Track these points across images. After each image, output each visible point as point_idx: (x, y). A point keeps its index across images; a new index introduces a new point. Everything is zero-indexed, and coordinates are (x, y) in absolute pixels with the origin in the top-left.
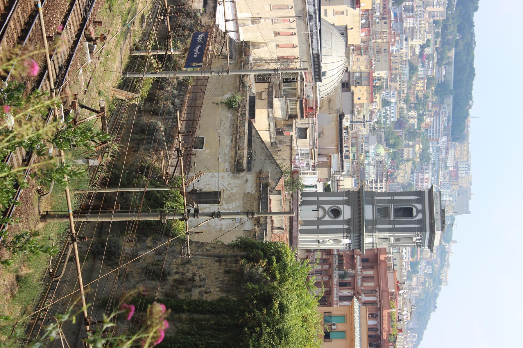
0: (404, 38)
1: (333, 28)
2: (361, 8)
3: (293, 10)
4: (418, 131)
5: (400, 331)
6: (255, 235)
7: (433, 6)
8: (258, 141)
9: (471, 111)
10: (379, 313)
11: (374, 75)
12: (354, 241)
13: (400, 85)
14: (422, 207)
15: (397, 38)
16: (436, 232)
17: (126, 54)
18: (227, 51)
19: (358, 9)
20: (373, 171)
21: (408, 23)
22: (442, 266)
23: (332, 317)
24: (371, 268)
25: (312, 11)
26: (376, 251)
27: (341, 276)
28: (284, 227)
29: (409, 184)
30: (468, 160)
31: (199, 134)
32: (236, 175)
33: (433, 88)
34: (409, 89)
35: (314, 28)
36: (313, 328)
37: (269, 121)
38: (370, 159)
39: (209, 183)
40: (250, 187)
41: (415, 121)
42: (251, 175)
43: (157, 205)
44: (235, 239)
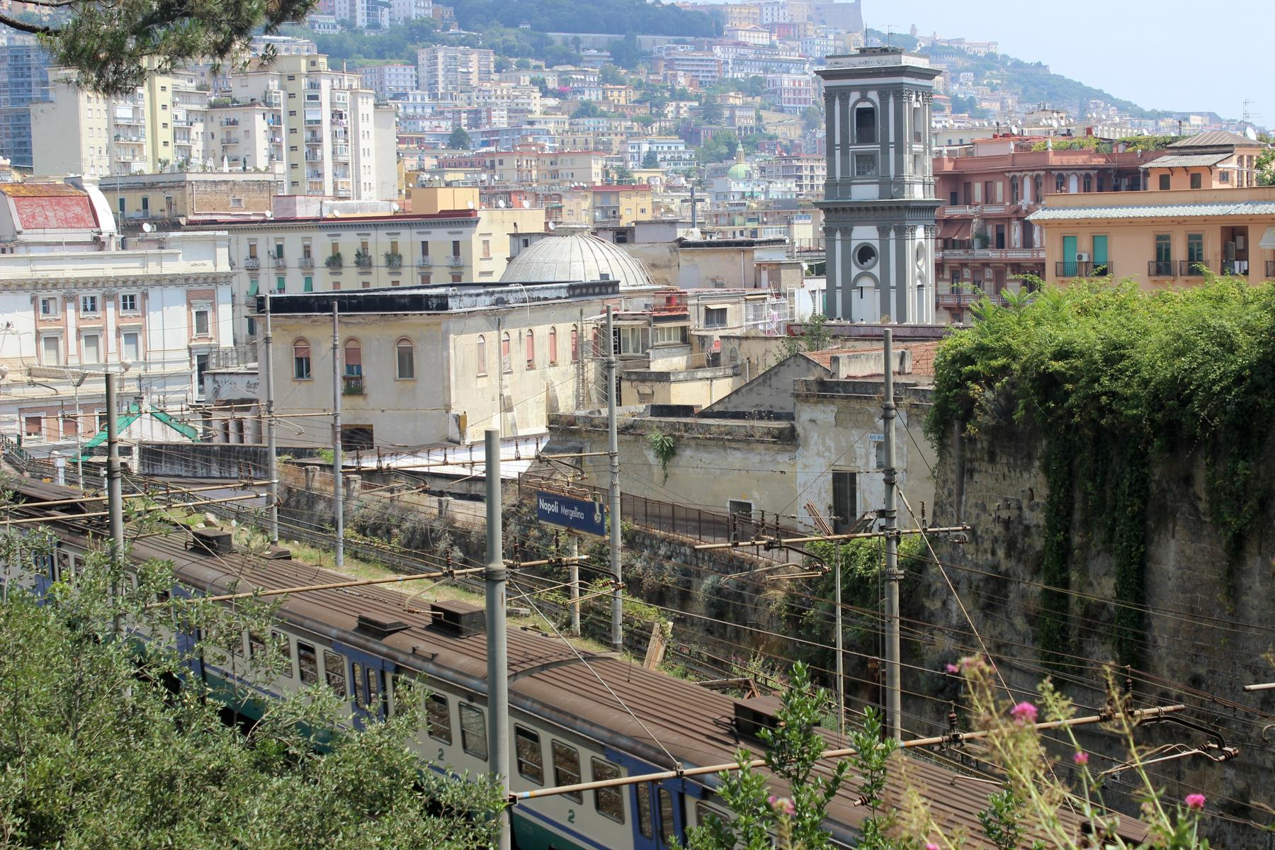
0: (529, 127)
1: (518, 260)
2: (477, 208)
3: (486, 334)
4: (703, 100)
5: (1089, 131)
6: (917, 406)
7: (469, 73)
8: (734, 398)
10: (1056, 173)
11: (599, 184)
13: (616, 135)
14: (855, 90)
15: (530, 140)
16: (903, 64)
18: (567, 457)
19: (479, 214)
20: (779, 185)
21: (500, 120)
22: (960, 53)
23: (1067, 260)
24: (968, 186)
26: (938, 178)
27: (985, 244)
28: (900, 351)
29: (805, 115)
31: (725, 510)
32: (801, 441)
34: (623, 116)
35: (519, 295)
36: (1099, 296)
37: (693, 379)
39: (817, 491)
40: (825, 416)
41: (685, 106)
42: (802, 414)
43: (862, 590)
44: (929, 443)
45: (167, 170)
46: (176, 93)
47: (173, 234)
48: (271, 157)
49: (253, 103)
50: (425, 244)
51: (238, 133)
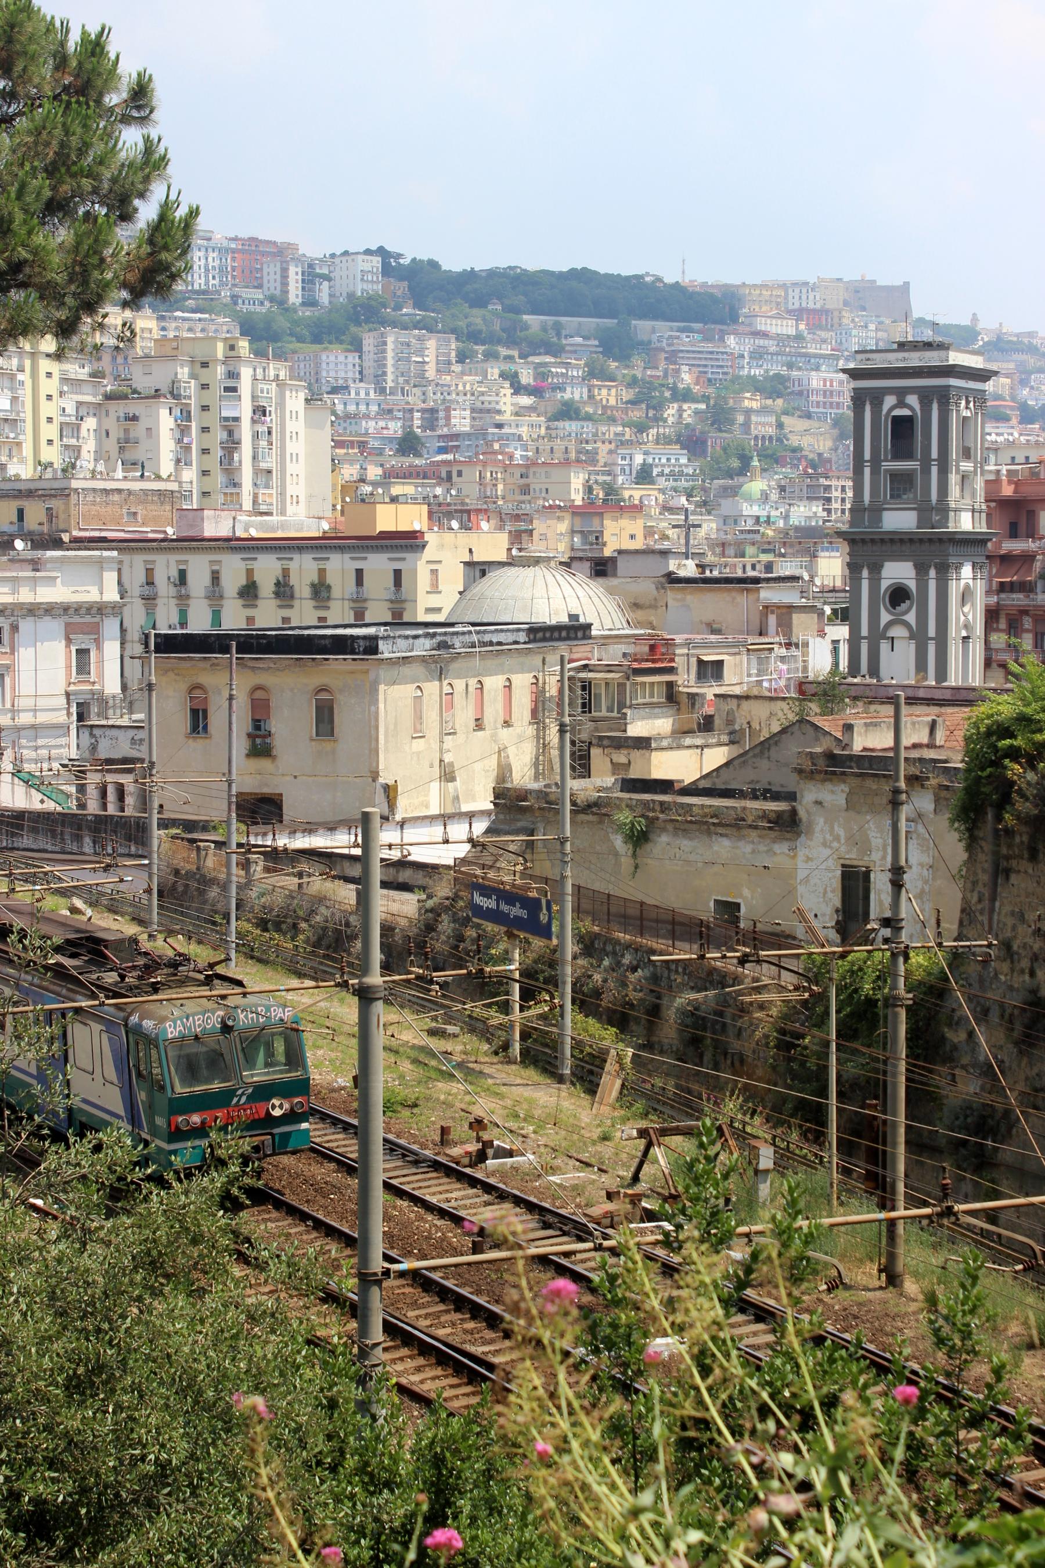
4: (712, 402)
9: (669, 279)
12: (966, 557)
17: (516, 1073)
21: (461, 421)
25: (428, 643)
30: (784, 286)
33: (614, 365)
34: (612, 420)
35: (467, 639)
37: (680, 747)
38: (773, 513)
41: (689, 408)
45: (49, 474)
46: (65, 380)
47: (50, 554)
48: (178, 461)
49: (157, 394)
50: (359, 573)
51: (138, 430)
